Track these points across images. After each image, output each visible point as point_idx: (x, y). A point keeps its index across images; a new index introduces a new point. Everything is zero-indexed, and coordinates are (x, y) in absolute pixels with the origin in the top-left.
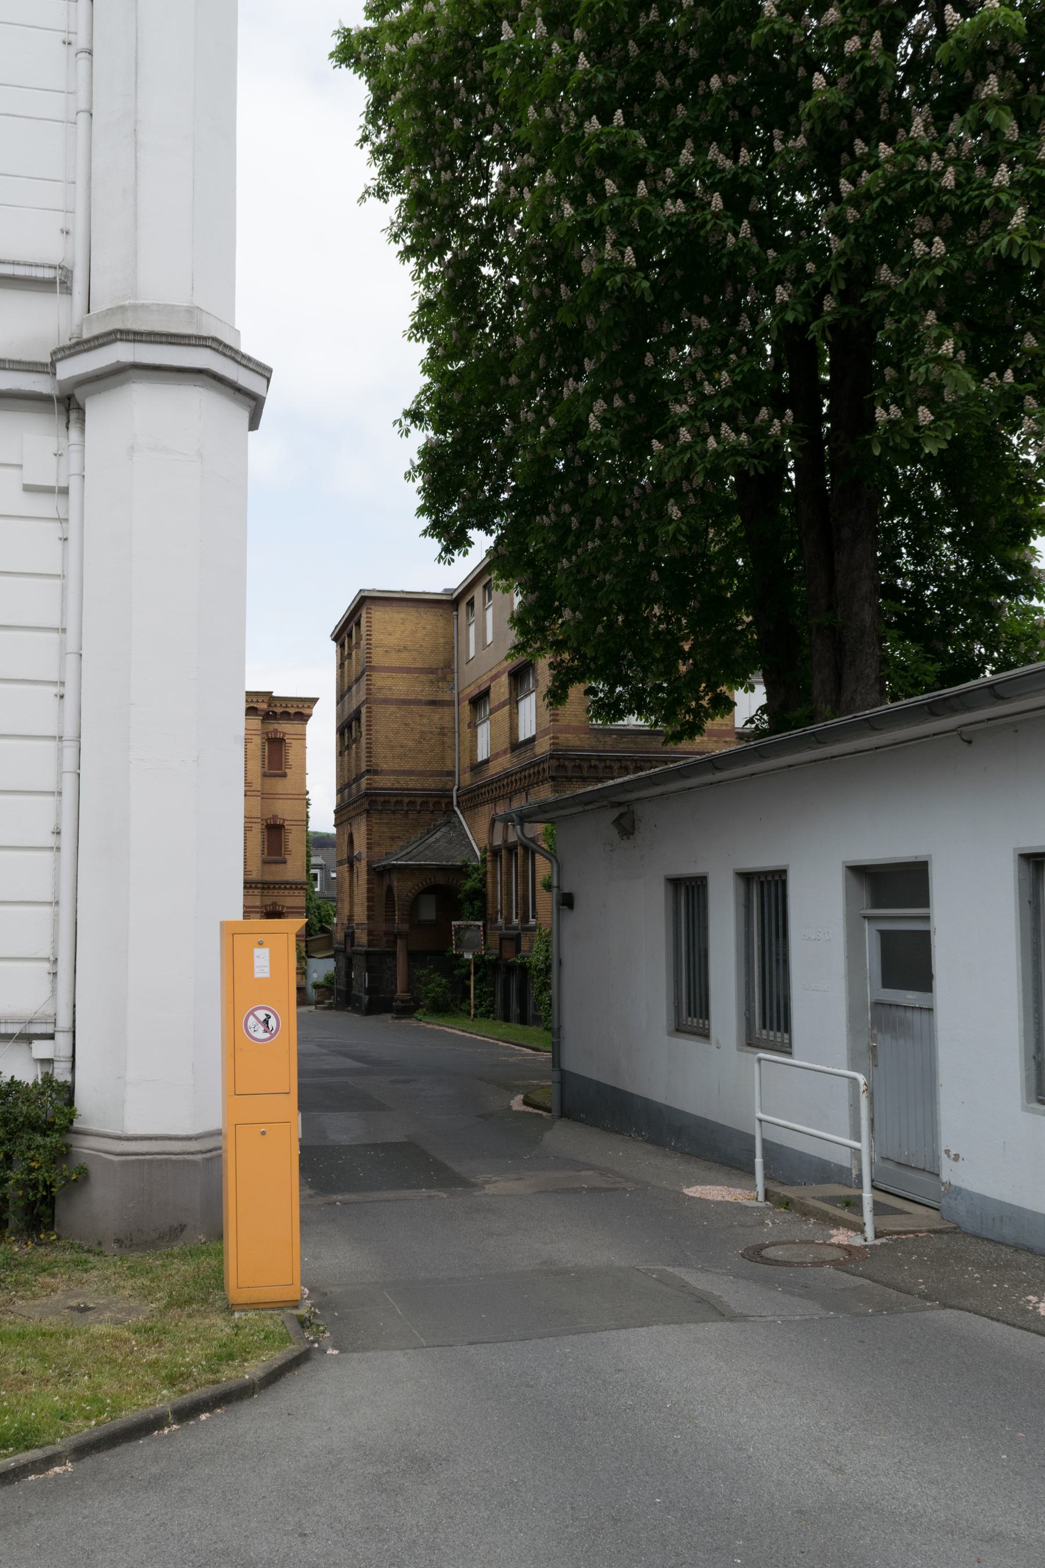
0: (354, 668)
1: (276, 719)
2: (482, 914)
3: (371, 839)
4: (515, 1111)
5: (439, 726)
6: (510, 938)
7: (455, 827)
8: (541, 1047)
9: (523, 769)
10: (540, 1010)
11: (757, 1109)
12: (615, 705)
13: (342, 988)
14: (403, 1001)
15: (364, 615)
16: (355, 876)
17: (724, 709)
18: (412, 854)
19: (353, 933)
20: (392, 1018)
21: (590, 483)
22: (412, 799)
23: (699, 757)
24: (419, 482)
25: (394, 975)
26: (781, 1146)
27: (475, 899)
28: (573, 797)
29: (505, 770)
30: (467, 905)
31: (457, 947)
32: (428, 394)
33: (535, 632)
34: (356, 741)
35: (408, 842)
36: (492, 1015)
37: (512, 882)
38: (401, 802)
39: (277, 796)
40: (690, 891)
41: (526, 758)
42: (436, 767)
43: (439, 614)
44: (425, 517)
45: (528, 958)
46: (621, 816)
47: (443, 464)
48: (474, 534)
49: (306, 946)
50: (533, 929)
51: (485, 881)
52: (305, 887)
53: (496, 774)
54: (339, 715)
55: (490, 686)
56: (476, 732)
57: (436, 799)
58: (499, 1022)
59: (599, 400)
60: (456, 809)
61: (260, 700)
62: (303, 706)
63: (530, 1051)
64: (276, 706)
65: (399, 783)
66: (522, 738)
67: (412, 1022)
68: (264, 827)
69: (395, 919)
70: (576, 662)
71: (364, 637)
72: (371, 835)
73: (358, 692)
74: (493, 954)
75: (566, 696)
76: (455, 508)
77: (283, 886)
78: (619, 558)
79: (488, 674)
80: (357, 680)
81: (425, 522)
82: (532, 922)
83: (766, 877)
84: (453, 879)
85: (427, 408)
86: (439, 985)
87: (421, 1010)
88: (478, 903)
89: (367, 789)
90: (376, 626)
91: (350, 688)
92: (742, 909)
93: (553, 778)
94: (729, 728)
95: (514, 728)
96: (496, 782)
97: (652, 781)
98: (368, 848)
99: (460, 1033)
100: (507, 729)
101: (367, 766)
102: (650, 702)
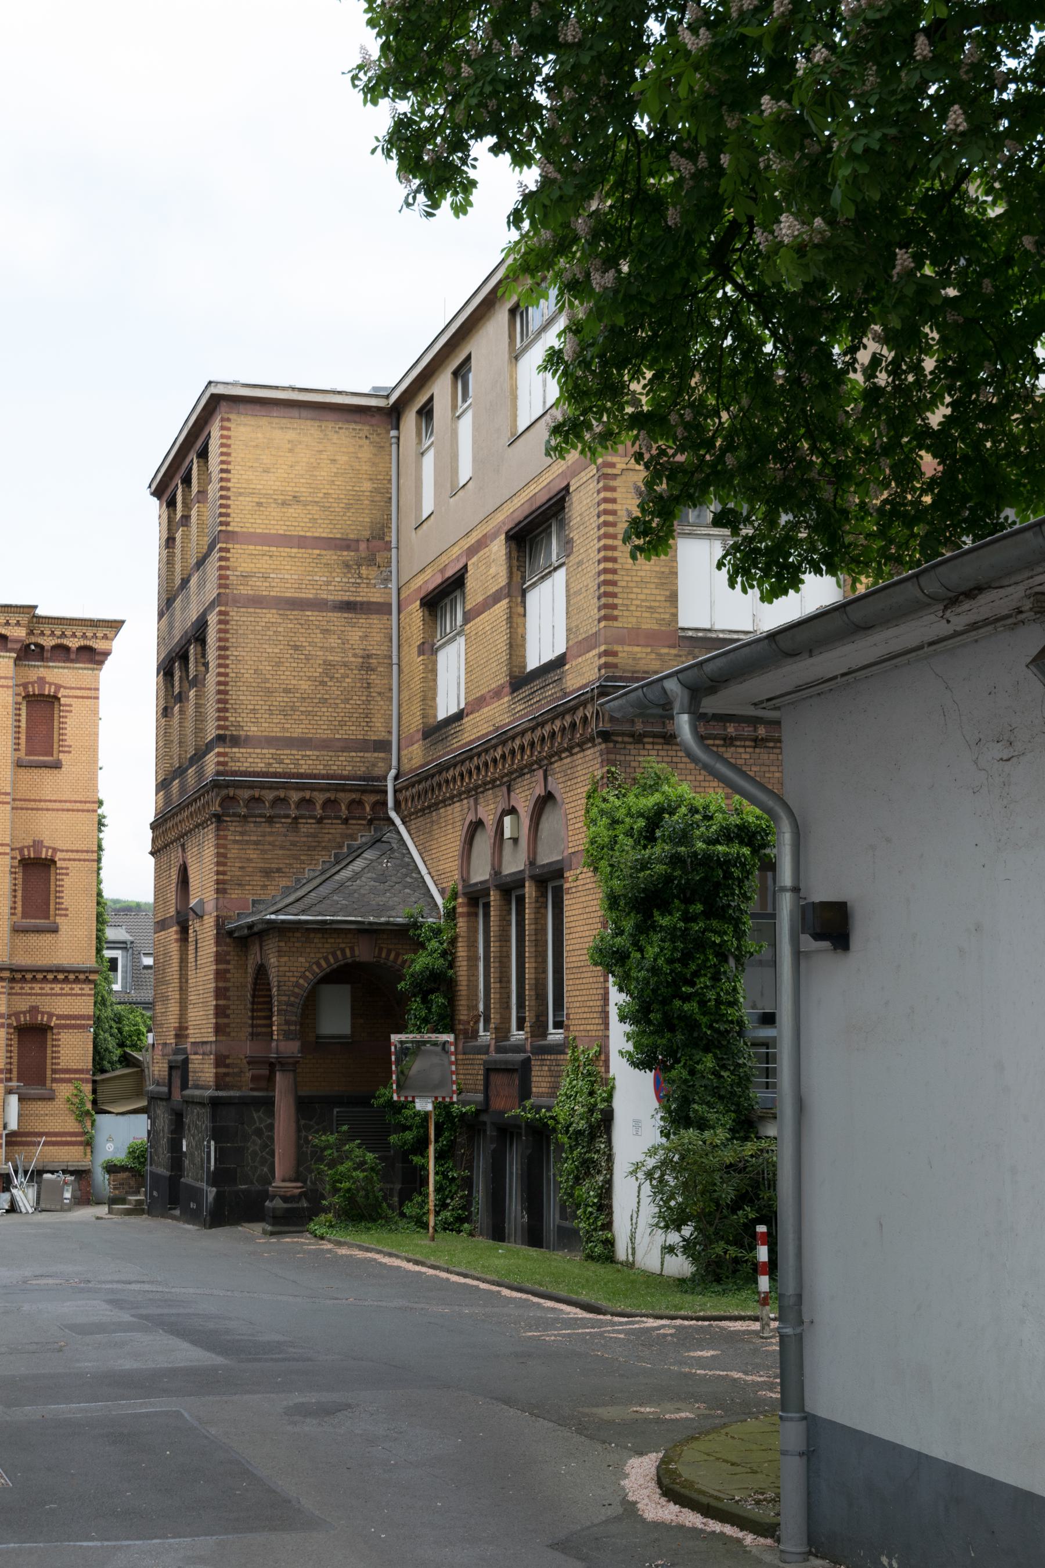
0: (194, 539)
1: (42, 659)
2: (447, 1021)
3: (224, 873)
5: (360, 652)
6: (507, 1070)
8: (603, 1303)
9: (538, 723)
10: (576, 1217)
13: (163, 1171)
14: (285, 1199)
16: (191, 947)
18: (307, 901)
19: (186, 1061)
20: (265, 1232)
22: (307, 795)
27: (432, 991)
30: (416, 1005)
34: (197, 682)
35: (298, 880)
36: (466, 1225)
37: (509, 957)
38: (284, 801)
39: (43, 805)
41: (546, 698)
42: (353, 732)
43: (362, 434)
49: (94, 1091)
50: (558, 1049)
52: (92, 977)
53: (478, 738)
54: (161, 640)
55: (465, 567)
56: (435, 663)
57: (354, 796)
60: (393, 814)
61: (13, 621)
62: (95, 636)
63: (581, 1314)
64: (42, 634)
67: (305, 1242)
68: (16, 863)
69: (271, 1034)
71: (215, 475)
72: (224, 864)
73: (202, 584)
74: (469, 1103)
77: (50, 976)
80: (201, 563)
82: (555, 1036)
84: (389, 952)
86: (360, 1166)
87: (322, 1217)
89: (218, 773)
90: (238, 454)
91: (185, 582)
93: (606, 736)
95: (516, 644)
96: (479, 755)
99: (410, 1267)
101: (219, 727)
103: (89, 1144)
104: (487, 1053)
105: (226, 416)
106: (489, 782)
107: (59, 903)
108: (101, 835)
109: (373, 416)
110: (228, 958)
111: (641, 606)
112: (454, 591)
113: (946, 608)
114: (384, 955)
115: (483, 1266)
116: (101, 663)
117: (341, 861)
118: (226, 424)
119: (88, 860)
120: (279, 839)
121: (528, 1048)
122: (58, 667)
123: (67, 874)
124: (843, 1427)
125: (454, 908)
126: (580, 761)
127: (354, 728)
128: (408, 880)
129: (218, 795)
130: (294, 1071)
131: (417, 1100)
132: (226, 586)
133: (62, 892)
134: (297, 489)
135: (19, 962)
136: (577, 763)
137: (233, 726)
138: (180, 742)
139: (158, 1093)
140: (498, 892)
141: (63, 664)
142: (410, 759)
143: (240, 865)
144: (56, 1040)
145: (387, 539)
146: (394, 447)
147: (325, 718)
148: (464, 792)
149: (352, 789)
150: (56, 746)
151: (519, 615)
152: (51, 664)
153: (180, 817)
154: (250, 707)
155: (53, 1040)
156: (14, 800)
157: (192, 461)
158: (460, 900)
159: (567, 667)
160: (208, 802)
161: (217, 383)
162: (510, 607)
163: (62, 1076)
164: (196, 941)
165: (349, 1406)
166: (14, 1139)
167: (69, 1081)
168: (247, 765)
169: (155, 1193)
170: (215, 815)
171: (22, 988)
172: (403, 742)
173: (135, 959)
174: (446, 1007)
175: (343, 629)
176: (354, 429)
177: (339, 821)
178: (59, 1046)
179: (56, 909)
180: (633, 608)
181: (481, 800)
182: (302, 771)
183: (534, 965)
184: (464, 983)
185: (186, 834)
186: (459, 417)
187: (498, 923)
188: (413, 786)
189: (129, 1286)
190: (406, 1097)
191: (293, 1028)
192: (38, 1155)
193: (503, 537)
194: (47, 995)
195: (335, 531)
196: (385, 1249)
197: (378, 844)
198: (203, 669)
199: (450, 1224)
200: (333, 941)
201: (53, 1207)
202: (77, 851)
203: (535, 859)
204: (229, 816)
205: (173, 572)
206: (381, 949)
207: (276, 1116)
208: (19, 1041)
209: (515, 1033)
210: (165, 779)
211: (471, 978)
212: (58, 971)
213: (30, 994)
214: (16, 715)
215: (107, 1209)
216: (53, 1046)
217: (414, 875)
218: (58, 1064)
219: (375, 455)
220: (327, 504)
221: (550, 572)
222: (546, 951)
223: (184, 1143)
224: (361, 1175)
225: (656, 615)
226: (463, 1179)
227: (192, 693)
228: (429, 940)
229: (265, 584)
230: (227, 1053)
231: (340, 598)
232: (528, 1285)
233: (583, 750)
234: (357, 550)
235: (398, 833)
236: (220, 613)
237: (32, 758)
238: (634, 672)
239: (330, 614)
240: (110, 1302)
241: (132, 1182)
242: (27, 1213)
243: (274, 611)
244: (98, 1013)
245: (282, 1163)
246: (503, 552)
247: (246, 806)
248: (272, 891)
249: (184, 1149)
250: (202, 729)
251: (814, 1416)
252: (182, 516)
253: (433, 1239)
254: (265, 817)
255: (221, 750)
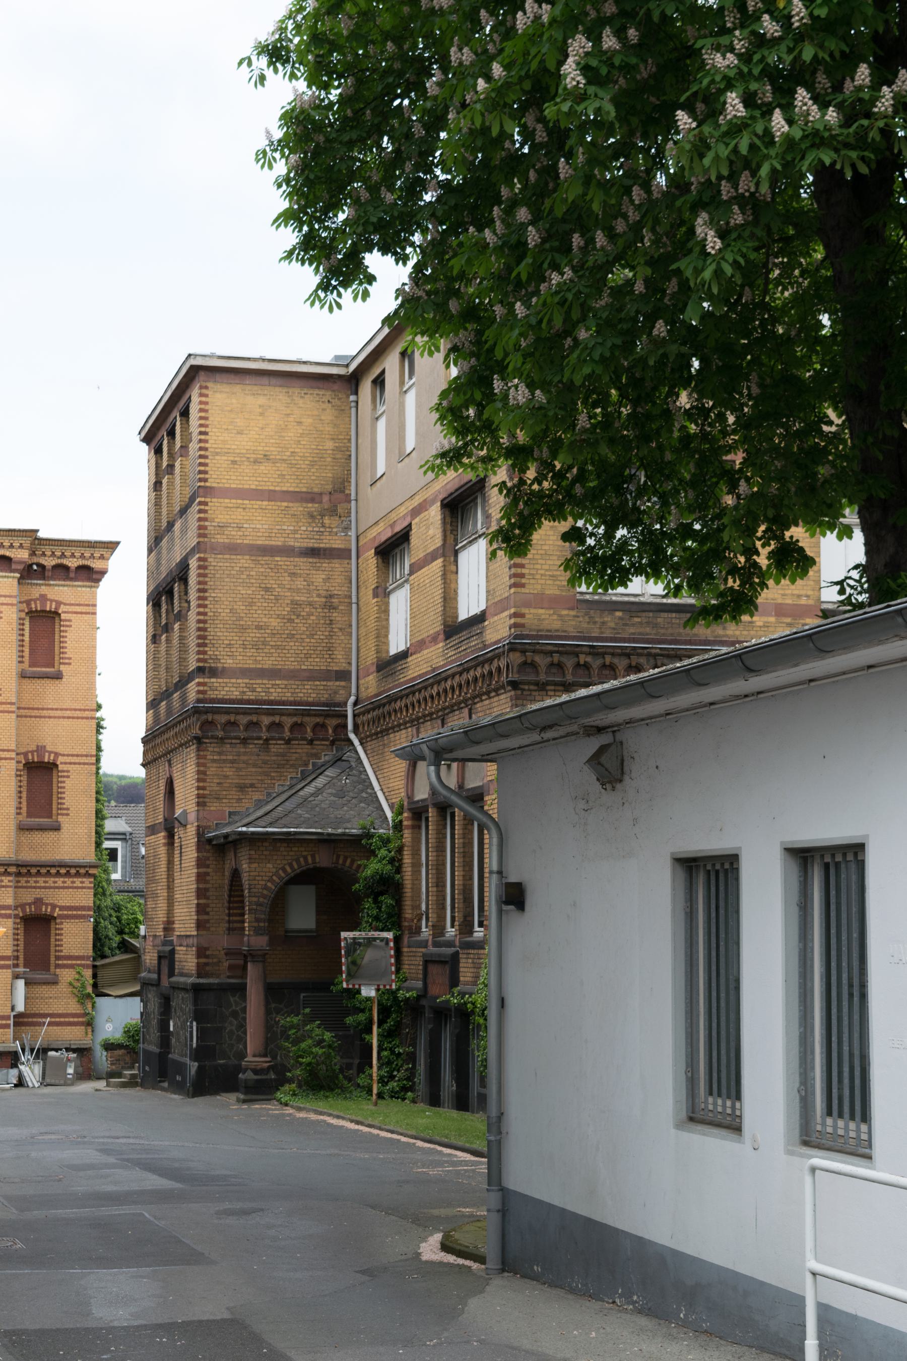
1: (44, 578)
3: (204, 788)
4: (427, 1262)
5: (324, 593)
6: (441, 962)
7: (350, 767)
9: (464, 669)
11: (809, 1255)
12: (612, 560)
13: (154, 1049)
14: (256, 1072)
15: (195, 399)
16: (177, 852)
17: (797, 567)
18: (274, 815)
19: (173, 952)
20: (238, 1100)
21: (562, 176)
22: (277, 719)
23: (725, 650)
24: (281, 168)
25: (242, 1026)
26: (855, 1318)
27: (382, 893)
28: (520, 716)
29: (434, 670)
30: (368, 904)
31: (350, 976)
32: (299, 18)
33: (479, 431)
34: (181, 616)
35: (269, 794)
36: (409, 1094)
37: (444, 864)
38: (257, 724)
39: (45, 713)
40: (713, 882)
41: (470, 648)
42: (317, 663)
43: (325, 399)
44: (291, 229)
45: (471, 995)
46: (602, 749)
47: (322, 139)
48: (374, 261)
49: (95, 976)
51: (400, 860)
52: (92, 871)
53: (420, 676)
54: (152, 573)
55: (410, 525)
56: (387, 604)
57: (318, 720)
58: (421, 1106)
59: (578, 36)
60: (352, 736)
61: (16, 544)
64: (44, 554)
65: (254, 691)
66: (463, 615)
67: (272, 1108)
68: (21, 766)
69: (243, 929)
70: (546, 484)
71: (195, 437)
72: (204, 781)
73: (184, 531)
75: (529, 542)
76: (342, 217)
77: (53, 871)
78: (603, 303)
79: (407, 504)
80: (183, 511)
81: (290, 237)
83: (833, 856)
85: (297, 40)
86: (319, 1043)
87: (287, 1087)
88: (387, 900)
89: (199, 701)
90: (215, 417)
91: (171, 525)
92: (795, 911)
93: (514, 685)
94: (811, 602)
95: (449, 598)
96: (420, 691)
97: (647, 691)
98: (198, 804)
100: (438, 599)
101: (199, 660)
102: (672, 556)
103: (90, 1024)
104: (426, 947)
105: (204, 384)
106: (428, 715)
107: (61, 804)
108: (100, 737)
109: (335, 382)
110: (208, 862)
111: (545, 575)
112: (402, 543)
113: (541, 732)
114: (341, 861)
115: (408, 1124)
116: (99, 580)
117: (306, 777)
118: (204, 391)
119: (87, 764)
120: (253, 758)
121: (457, 944)
122: (59, 585)
123: (68, 777)
124: (520, 1193)
125: (401, 821)
126: (496, 704)
127: (318, 660)
128: (364, 795)
129: (198, 720)
130: (264, 962)
131: (362, 988)
132: (205, 536)
133: (64, 793)
134: (267, 449)
135: (24, 858)
136: (494, 705)
137: (211, 659)
138: (167, 668)
139: (150, 979)
140: (435, 810)
141: (63, 583)
142: (367, 688)
143: (218, 781)
144: (59, 929)
145: (347, 492)
146: (353, 410)
147: (292, 651)
148: (408, 722)
149: (317, 714)
150: (57, 658)
151: (452, 572)
152: (52, 582)
153: (166, 736)
154: (226, 642)
155: (56, 929)
156: (19, 708)
157: (176, 418)
158: (405, 815)
159: (486, 623)
160: (189, 726)
161: (196, 355)
162: (444, 566)
163: (65, 962)
164: (181, 846)
165: (262, 1210)
166: (21, 1020)
167: (71, 966)
168: (224, 693)
169: (147, 1068)
170: (195, 738)
171: (27, 882)
172: (361, 672)
173: (134, 850)
174: (394, 907)
175: (308, 572)
176: (318, 394)
177: (305, 742)
178: (61, 935)
179: (58, 809)
180: (538, 577)
181: (422, 730)
182: (272, 698)
183: (462, 873)
184: (409, 886)
185: (172, 751)
186: (406, 392)
187: (435, 836)
188: (369, 712)
189: (117, 1141)
190: (354, 985)
191: (262, 924)
192: (43, 1034)
193: (439, 504)
194: (50, 888)
195: (301, 485)
196: (335, 1113)
197: (339, 762)
198: (186, 605)
199: (396, 1092)
200: (296, 849)
201: (57, 1082)
202: (77, 756)
203: (463, 783)
204: (207, 738)
205: (160, 515)
206: (338, 857)
207: (248, 1001)
208: (25, 930)
209: (449, 930)
210: (154, 700)
211: (416, 882)
212: (60, 866)
213: (35, 887)
214: (20, 629)
215: (105, 1084)
216: (56, 935)
217: (369, 791)
218: (61, 951)
219: (336, 417)
220: (293, 462)
221: (476, 538)
222: (472, 861)
223: (171, 1024)
224: (320, 1051)
225: (558, 583)
226: (408, 1054)
227: (176, 626)
228: (379, 849)
229: (239, 533)
230: (206, 945)
231: (305, 545)
232: (438, 1138)
233: (498, 695)
234: (321, 502)
235: (356, 752)
236: (200, 559)
237: (35, 669)
238: (538, 631)
239: (296, 559)
240: (101, 1151)
241: (128, 1059)
242: (34, 1087)
243: (247, 557)
244: (98, 902)
245: (253, 1041)
246: (439, 517)
247: (223, 730)
248: (246, 804)
249: (171, 1029)
250: (185, 659)
251: (508, 1189)
252: (168, 465)
253: (376, 1104)
254: (239, 739)
255: (201, 680)
